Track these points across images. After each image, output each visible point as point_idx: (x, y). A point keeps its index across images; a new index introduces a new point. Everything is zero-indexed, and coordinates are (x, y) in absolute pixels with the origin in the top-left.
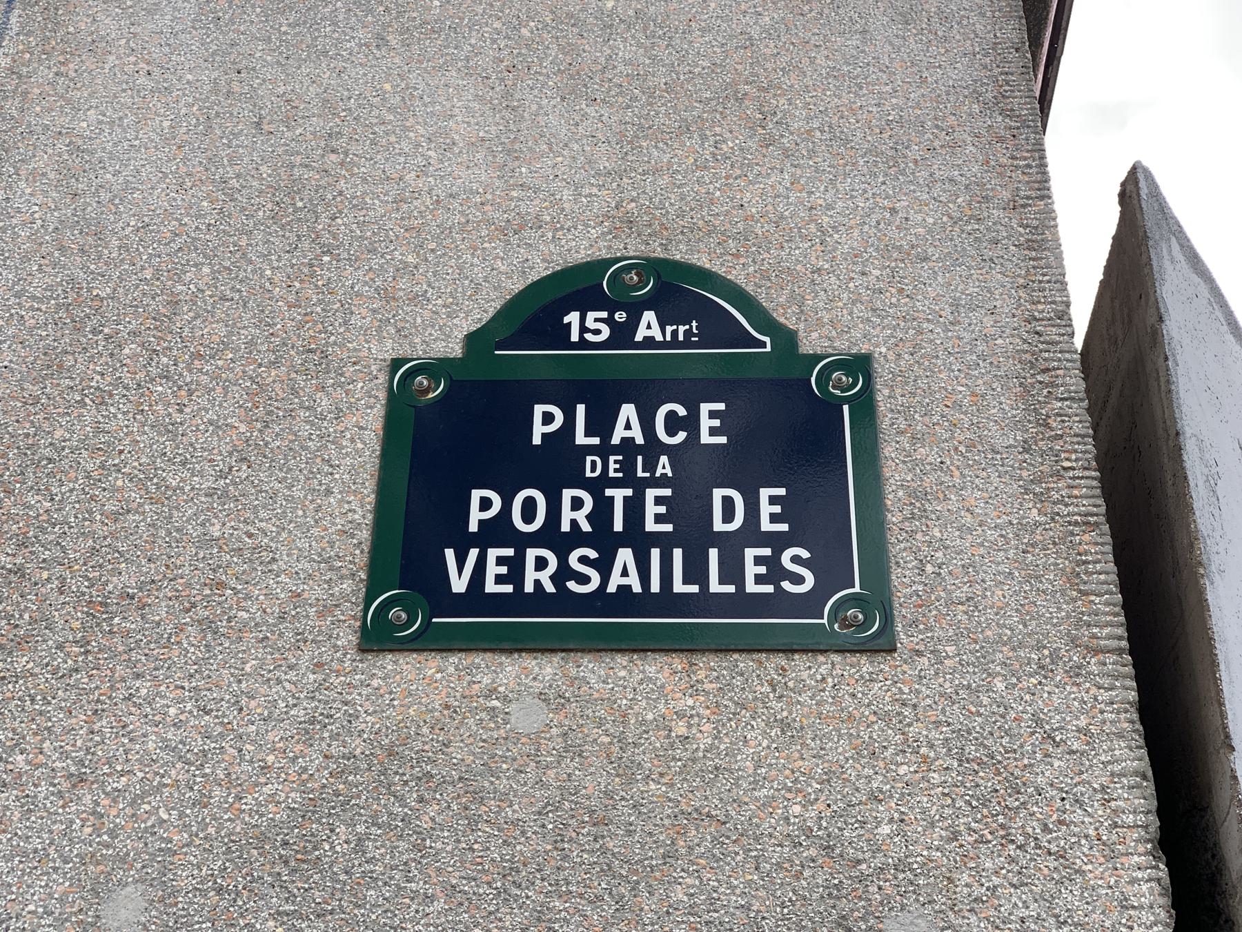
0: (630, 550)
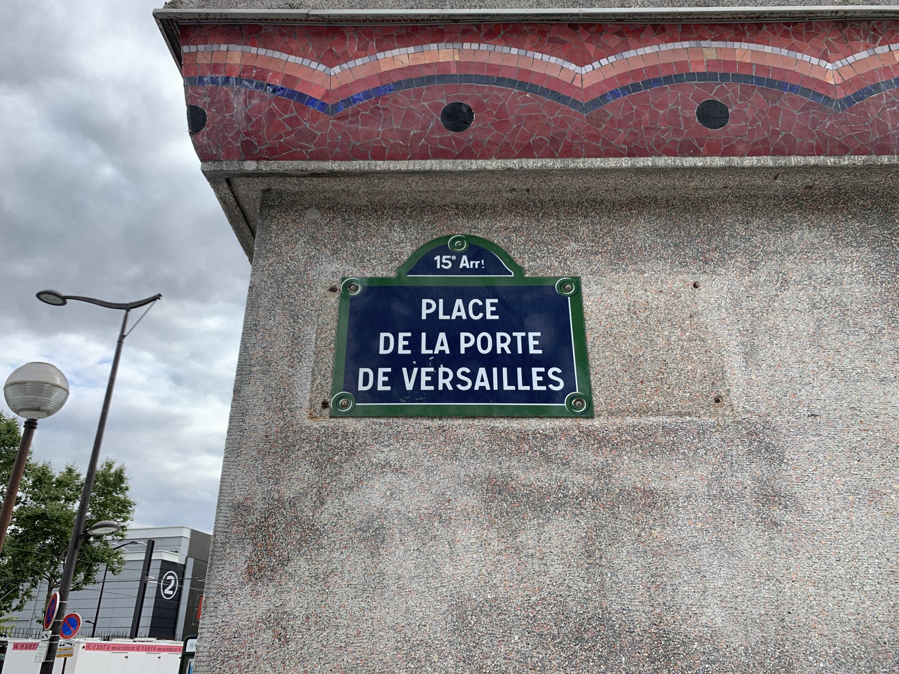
0: (484, 368)
